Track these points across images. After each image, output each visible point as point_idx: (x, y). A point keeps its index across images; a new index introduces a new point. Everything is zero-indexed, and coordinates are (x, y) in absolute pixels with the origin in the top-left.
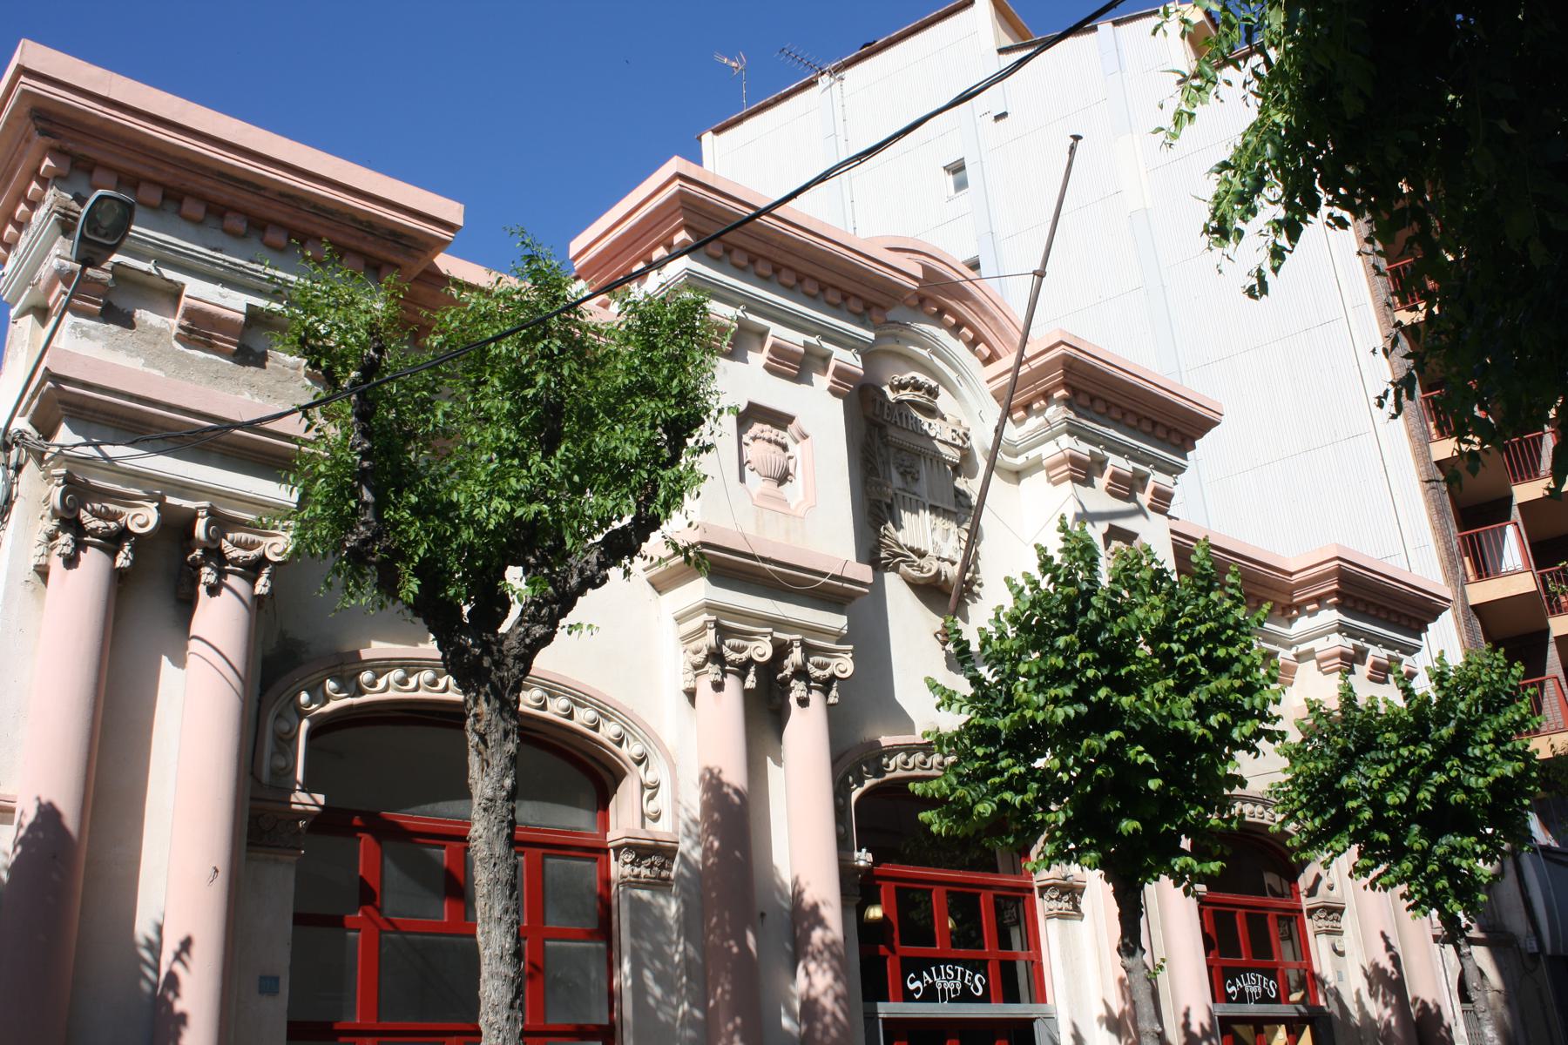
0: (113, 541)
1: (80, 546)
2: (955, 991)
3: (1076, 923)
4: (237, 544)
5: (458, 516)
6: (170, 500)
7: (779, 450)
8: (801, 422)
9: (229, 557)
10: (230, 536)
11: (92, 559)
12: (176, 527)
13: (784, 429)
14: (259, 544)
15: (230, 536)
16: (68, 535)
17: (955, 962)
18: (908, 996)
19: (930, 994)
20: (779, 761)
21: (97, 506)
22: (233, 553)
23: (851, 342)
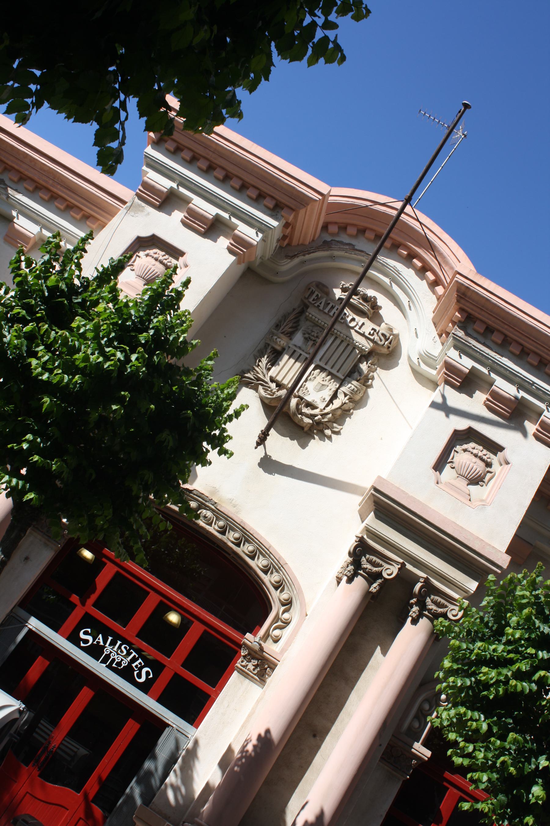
0: (372, 577)
2: (119, 664)
4: (369, 561)
6: (409, 567)
7: (482, 464)
8: (507, 453)
10: (432, 597)
12: (405, 579)
13: (495, 454)
14: (446, 607)
15: (368, 556)
18: (74, 639)
19: (95, 651)
20: (384, 652)
22: (431, 606)
23: (258, 225)
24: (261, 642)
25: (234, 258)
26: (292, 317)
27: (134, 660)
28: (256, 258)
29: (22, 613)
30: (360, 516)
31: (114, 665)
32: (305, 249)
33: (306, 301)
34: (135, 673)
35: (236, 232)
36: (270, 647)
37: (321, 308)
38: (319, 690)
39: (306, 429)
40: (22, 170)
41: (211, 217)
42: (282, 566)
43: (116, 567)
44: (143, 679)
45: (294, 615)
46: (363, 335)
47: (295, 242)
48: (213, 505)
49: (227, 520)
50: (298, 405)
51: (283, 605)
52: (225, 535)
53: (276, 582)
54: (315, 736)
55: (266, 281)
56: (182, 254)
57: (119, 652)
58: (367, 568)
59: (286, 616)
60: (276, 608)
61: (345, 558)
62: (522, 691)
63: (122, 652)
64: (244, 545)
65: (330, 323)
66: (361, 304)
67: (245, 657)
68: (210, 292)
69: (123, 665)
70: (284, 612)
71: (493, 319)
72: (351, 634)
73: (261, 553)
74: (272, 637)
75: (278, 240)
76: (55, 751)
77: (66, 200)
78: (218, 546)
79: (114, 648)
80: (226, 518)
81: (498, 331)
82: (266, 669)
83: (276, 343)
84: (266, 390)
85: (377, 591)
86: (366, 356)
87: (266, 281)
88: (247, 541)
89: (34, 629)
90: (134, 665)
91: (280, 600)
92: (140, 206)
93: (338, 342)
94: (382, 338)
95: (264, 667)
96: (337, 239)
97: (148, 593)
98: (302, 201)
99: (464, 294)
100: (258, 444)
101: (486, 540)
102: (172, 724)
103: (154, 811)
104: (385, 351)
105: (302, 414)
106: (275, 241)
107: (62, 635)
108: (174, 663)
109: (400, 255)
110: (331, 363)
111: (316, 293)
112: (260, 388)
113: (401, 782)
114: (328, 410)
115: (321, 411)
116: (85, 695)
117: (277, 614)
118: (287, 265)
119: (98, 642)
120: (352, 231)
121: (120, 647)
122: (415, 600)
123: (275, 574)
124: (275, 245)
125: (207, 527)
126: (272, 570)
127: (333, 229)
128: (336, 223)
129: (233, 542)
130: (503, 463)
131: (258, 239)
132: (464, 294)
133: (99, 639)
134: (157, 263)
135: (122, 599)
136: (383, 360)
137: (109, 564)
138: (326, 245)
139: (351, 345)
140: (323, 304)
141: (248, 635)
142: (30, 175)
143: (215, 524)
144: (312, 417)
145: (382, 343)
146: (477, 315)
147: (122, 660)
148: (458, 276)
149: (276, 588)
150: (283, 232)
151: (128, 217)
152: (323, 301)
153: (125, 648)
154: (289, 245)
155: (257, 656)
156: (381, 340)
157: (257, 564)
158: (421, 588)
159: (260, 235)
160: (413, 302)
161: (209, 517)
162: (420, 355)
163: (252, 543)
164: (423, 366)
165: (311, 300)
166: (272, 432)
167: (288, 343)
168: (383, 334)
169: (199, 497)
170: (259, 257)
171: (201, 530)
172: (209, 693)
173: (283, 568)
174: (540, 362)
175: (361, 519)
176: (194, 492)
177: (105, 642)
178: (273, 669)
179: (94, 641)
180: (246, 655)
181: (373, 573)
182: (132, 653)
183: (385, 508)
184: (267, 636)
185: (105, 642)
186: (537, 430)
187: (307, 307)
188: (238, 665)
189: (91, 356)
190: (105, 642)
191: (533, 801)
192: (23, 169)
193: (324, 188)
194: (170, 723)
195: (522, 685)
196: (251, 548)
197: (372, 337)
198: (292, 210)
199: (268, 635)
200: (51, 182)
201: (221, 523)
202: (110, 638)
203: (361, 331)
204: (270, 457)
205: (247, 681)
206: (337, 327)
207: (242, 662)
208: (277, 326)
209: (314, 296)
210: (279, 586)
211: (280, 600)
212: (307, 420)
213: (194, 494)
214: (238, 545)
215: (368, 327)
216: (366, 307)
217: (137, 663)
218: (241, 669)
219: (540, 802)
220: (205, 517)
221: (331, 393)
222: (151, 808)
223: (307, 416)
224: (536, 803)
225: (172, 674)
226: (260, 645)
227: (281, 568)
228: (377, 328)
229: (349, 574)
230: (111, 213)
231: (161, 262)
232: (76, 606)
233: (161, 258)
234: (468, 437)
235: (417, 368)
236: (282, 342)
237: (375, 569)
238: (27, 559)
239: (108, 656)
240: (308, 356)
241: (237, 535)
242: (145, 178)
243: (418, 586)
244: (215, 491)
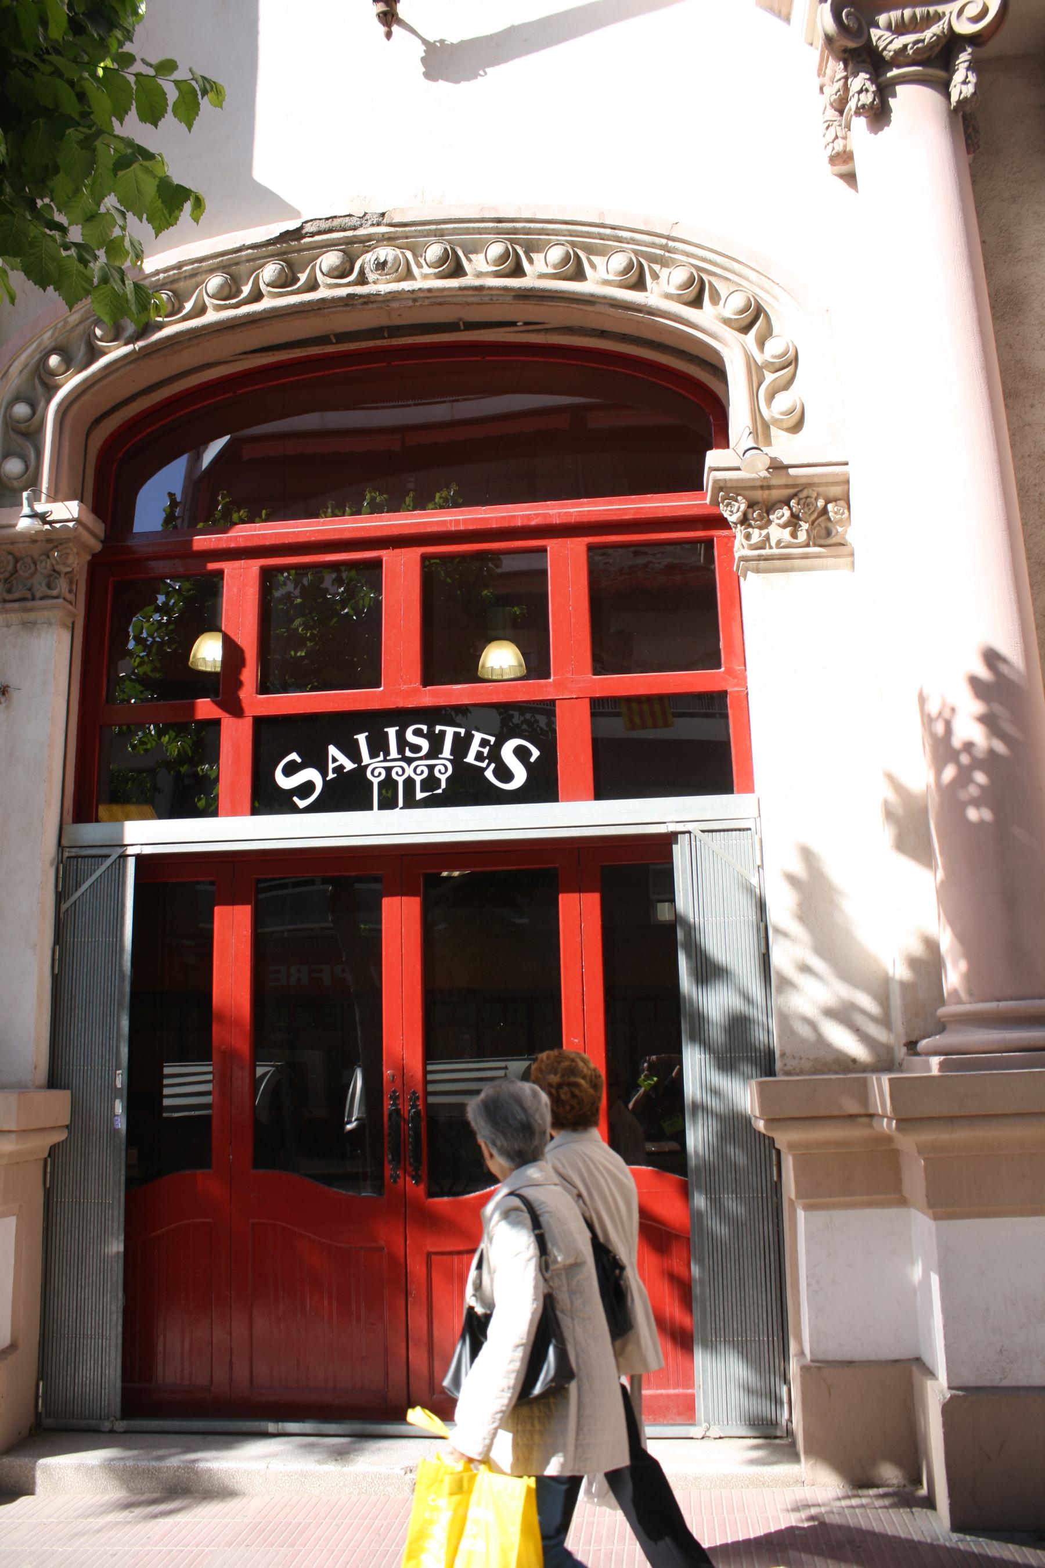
0: (937, 60)
1: (884, 91)
2: (431, 782)
4: (900, 29)
5: (121, 44)
9: (888, 55)
10: (882, 19)
11: (915, 105)
16: (863, 76)
18: (268, 799)
19: (347, 793)
21: (894, 15)
27: (461, 745)
29: (91, 833)
30: (770, 9)
31: (420, 795)
34: (489, 774)
42: (668, 238)
43: (250, 562)
44: (520, 776)
48: (379, 224)
49: (441, 234)
51: (745, 329)
52: (465, 274)
57: (408, 754)
58: (905, 46)
59: (774, 348)
60: (734, 352)
63: (416, 749)
64: (531, 261)
67: (744, 521)
69: (443, 779)
70: (761, 344)
73: (590, 250)
74: (776, 422)
76: (427, 1105)
79: (387, 753)
80: (436, 229)
82: (825, 511)
85: (976, 85)
88: (531, 248)
89: (148, 850)
90: (470, 759)
91: (727, 322)
95: (809, 507)
102: (679, 828)
103: (801, 1072)
116: (400, 919)
117: (749, 360)
119: (339, 769)
121: (402, 743)
125: (407, 285)
126: (650, 267)
129: (497, 275)
133: (335, 760)
137: (228, 567)
141: (713, 457)
143: (420, 266)
147: (431, 768)
153: (417, 733)
155: (776, 494)
161: (390, 259)
163: (549, 241)
169: (330, 231)
173: (674, 239)
175: (779, 15)
176: (309, 228)
178: (846, 499)
179: (324, 773)
180: (745, 514)
181: (931, 46)
182: (443, 733)
184: (762, 429)
190: (353, 754)
194: (672, 828)
199: (766, 426)
201: (434, 251)
202: (362, 738)
204: (442, 41)
207: (748, 537)
211: (727, 322)
213: (313, 234)
218: (760, 558)
220: (381, 266)
222: (788, 1073)
225: (585, 708)
227: (671, 244)
232: (217, 723)
239: (389, 784)
241: (496, 250)
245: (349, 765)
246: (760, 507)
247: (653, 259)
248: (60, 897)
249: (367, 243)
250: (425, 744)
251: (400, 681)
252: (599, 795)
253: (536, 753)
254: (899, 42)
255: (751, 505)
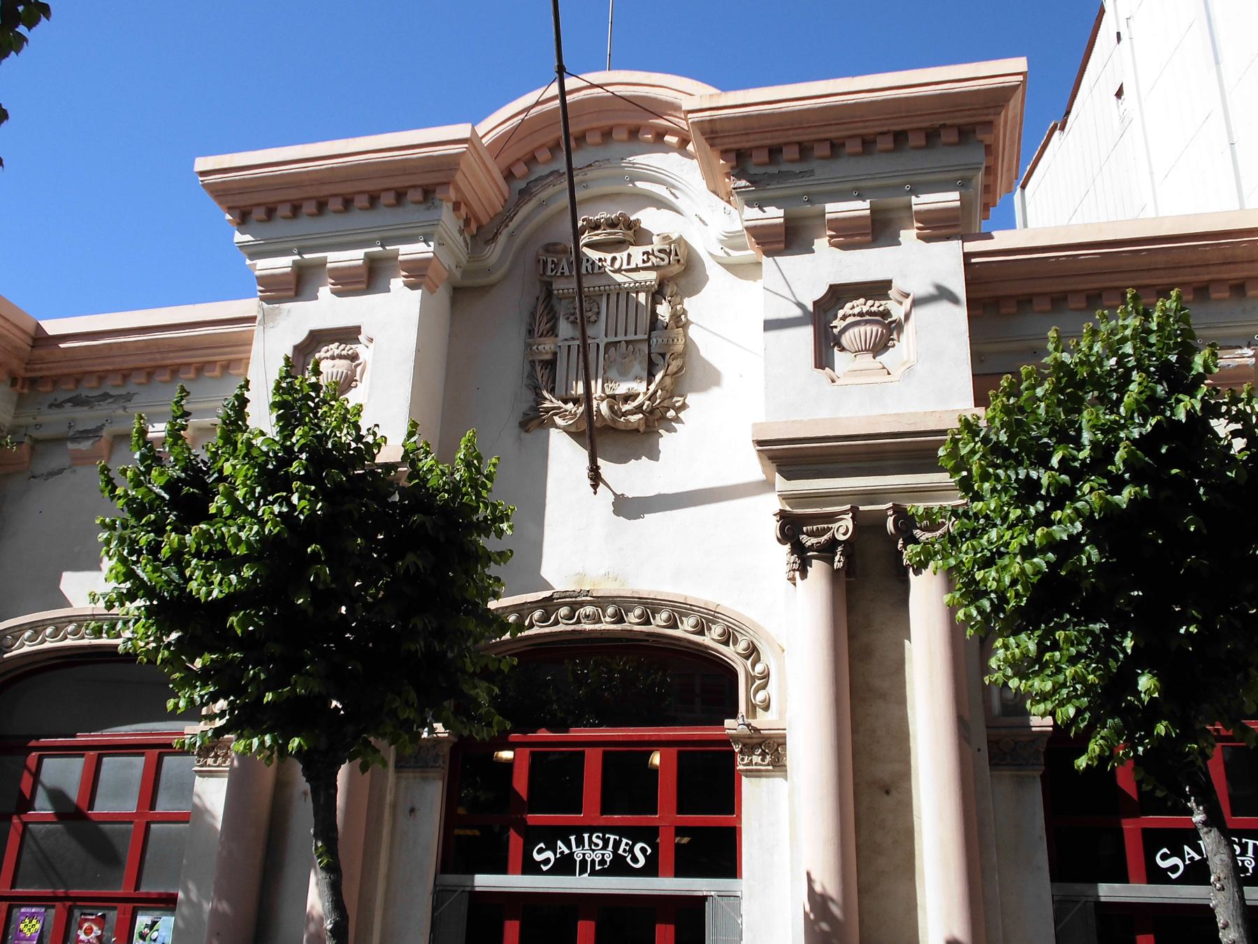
0: (827, 551)
2: (603, 862)
3: (777, 782)
7: (345, 362)
12: (867, 526)
17: (605, 830)
18: (531, 868)
19: (565, 866)
24: (750, 721)
25: (420, 291)
26: (540, 309)
27: (617, 844)
28: (450, 271)
31: (598, 868)
32: (504, 218)
33: (545, 279)
34: (628, 859)
35: (400, 258)
36: (763, 721)
37: (567, 273)
38: (854, 731)
39: (642, 429)
40: (118, 367)
41: (361, 262)
45: (768, 659)
46: (637, 269)
47: (485, 220)
50: (611, 408)
51: (747, 658)
53: (721, 635)
54: (887, 792)
55: (483, 290)
56: (887, 284)
59: (759, 668)
60: (741, 667)
61: (784, 551)
62: (1038, 572)
63: (597, 845)
65: (575, 285)
66: (610, 234)
67: (741, 752)
68: (418, 350)
70: (753, 666)
71: (769, 135)
72: (851, 637)
75: (461, 232)
77: (190, 364)
78: (628, 640)
81: (787, 144)
83: (541, 353)
84: (563, 417)
86: (657, 294)
87: (483, 290)
90: (620, 852)
92: (273, 309)
93: (613, 298)
94: (662, 255)
95: (771, 748)
96: (533, 178)
97: (583, 752)
98: (447, 166)
99: (713, 132)
100: (595, 486)
101: (940, 409)
104: (676, 269)
105: (625, 414)
106: (457, 235)
107: (514, 873)
108: (666, 816)
109: (647, 142)
110: (621, 330)
111: (550, 260)
112: (556, 418)
113: (1039, 780)
114: (652, 387)
115: (645, 394)
117: (747, 672)
118: (494, 253)
119: (1191, 859)
120: (543, 155)
122: (901, 541)
123: (713, 627)
124: (461, 239)
125: (597, 627)
127: (519, 170)
128: (518, 160)
129: (638, 624)
130: (901, 299)
131: (432, 249)
132: (713, 132)
134: (337, 361)
135: (557, 780)
136: (682, 282)
138: (525, 194)
139: (625, 294)
140: (566, 267)
142: (131, 366)
144: (639, 409)
145: (667, 261)
146: (747, 145)
148: (690, 116)
149: (726, 643)
150: (459, 218)
151: (270, 332)
152: (564, 263)
153: (598, 837)
154: (480, 227)
155: (755, 741)
156: (663, 260)
157: (684, 631)
158: (895, 522)
159: (431, 243)
160: (674, 187)
162: (721, 241)
164: (734, 253)
165: (549, 273)
166: (600, 462)
167: (555, 344)
168: (660, 251)
170: (453, 267)
171: (593, 635)
172: (732, 825)
174: (864, 143)
177: (570, 847)
183: (789, 457)
185: (570, 847)
186: (918, 228)
187: (550, 284)
188: (740, 767)
189: (241, 534)
190: (569, 846)
191: (1146, 698)
192: (119, 363)
193: (462, 131)
195: (1032, 564)
196: (664, 615)
197: (649, 264)
198: (447, 184)
200: (158, 356)
201: (610, 610)
202: (573, 838)
203: (633, 266)
205: (764, 780)
206: (586, 283)
208: (530, 332)
209: (550, 266)
210: (728, 638)
212: (634, 418)
214: (648, 622)
215: (637, 253)
216: (619, 234)
217: (623, 846)
219: (1156, 695)
220: (587, 617)
221: (646, 365)
223: (632, 412)
224: (1152, 699)
226: (748, 725)
228: (648, 248)
229: (796, 566)
230: (245, 343)
231: (340, 357)
233: (337, 352)
234: (838, 299)
235: (728, 260)
236: (547, 347)
237: (823, 539)
238: (412, 810)
239: (584, 862)
240: (578, 342)
241: (638, 611)
242: (257, 273)
243: (890, 521)
244: (581, 576)
245: (567, 851)
246: (749, 748)
247: (708, 621)
248: (434, 909)
249: (582, 604)
250: (600, 843)
251: (590, 811)
252: (676, 876)
253: (649, 851)
254: (814, 540)
255: (744, 745)
